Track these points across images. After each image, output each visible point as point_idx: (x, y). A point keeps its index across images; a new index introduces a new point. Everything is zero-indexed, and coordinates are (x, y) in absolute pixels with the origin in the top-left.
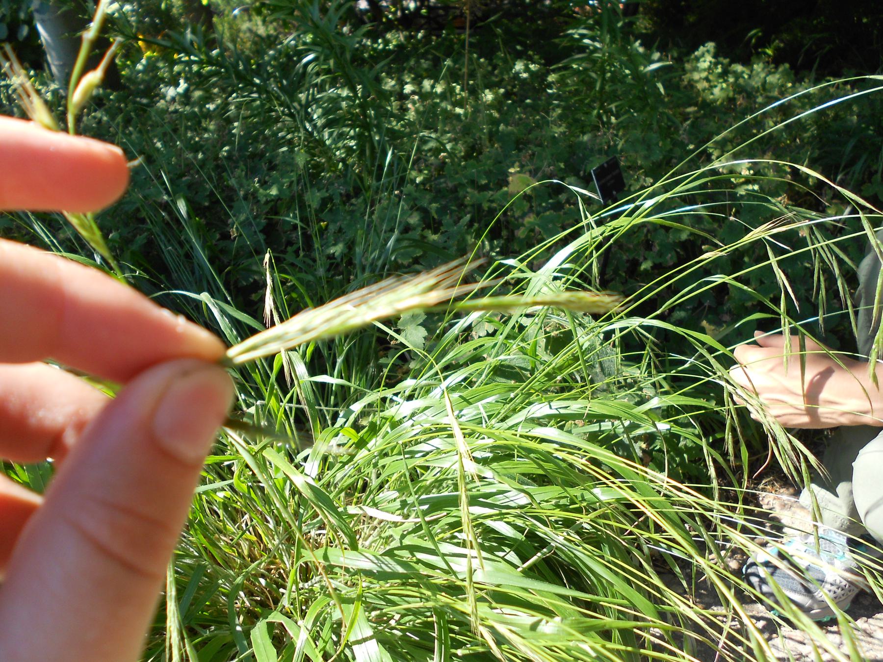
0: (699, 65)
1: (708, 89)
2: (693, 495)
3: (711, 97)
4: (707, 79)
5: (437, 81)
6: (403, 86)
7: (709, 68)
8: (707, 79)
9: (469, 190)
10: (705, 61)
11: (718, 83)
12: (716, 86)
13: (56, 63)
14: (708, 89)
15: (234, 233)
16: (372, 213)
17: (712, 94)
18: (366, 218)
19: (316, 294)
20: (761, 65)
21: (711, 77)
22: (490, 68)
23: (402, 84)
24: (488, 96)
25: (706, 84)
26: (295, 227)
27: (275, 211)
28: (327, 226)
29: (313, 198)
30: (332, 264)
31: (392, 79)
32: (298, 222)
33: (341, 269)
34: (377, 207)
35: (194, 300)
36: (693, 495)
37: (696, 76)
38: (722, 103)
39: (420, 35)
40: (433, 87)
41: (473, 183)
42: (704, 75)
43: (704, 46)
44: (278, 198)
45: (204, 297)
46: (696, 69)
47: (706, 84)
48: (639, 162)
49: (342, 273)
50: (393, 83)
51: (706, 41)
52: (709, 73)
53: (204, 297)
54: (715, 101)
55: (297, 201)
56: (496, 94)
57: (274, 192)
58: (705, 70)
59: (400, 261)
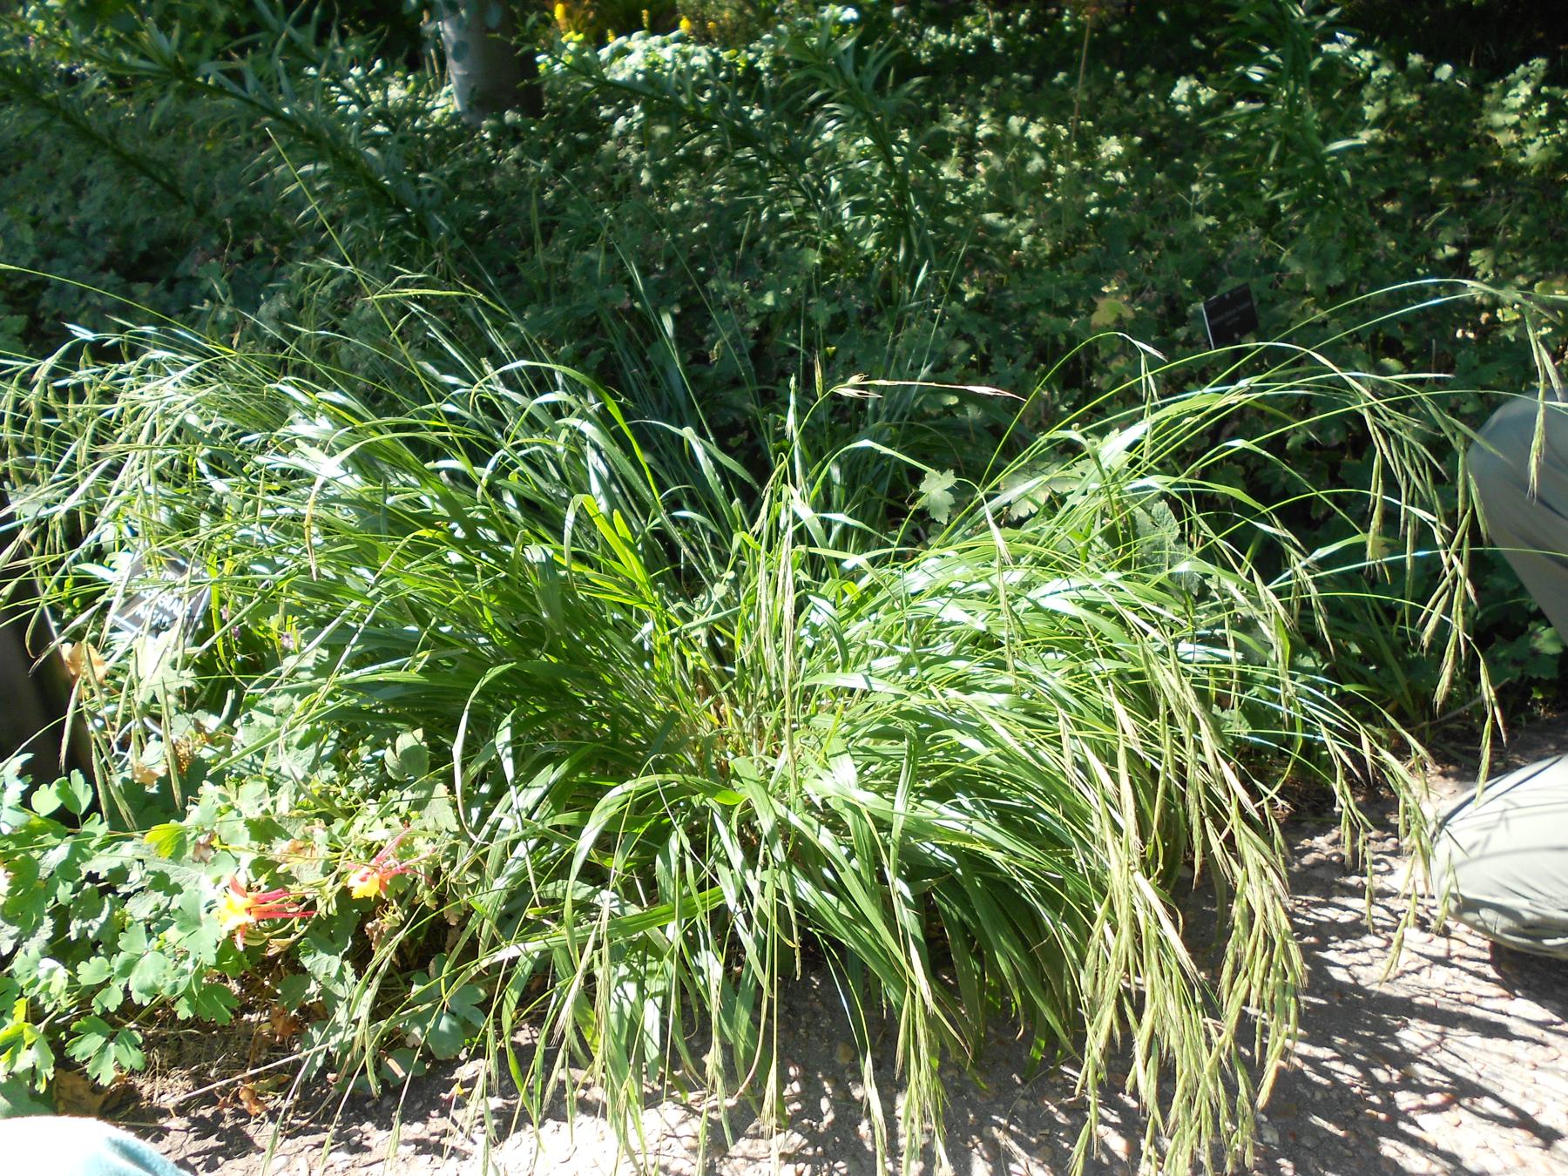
0: (1505, 101)
1: (1518, 147)
2: (1493, 1011)
3: (1521, 160)
4: (1517, 128)
5: (1032, 119)
6: (976, 125)
7: (1526, 107)
8: (1517, 128)
9: (1041, 314)
10: (1517, 95)
11: (1538, 134)
12: (1531, 142)
13: (459, 72)
14: (1518, 147)
15: (714, 355)
16: (895, 342)
17: (1523, 154)
18: (888, 347)
19: (814, 443)
20: (189, 684)
21: (1523, 124)
22: (1128, 93)
23: (976, 121)
24: (1112, 147)
25: (1512, 137)
26: (793, 352)
27: (766, 329)
28: (835, 352)
29: (822, 312)
30: (836, 407)
31: (958, 112)
32: (801, 349)
33: (848, 414)
34: (904, 332)
35: (673, 434)
36: (1493, 1011)
37: (1498, 118)
38: (1539, 173)
39: (1023, 17)
40: (1024, 128)
41: (1048, 304)
42: (1513, 118)
43: (1527, 65)
44: (773, 311)
45: (688, 433)
46: (1500, 107)
47: (1512, 137)
48: (1308, 286)
49: (849, 420)
50: (960, 119)
51: (1533, 56)
52: (1523, 117)
53: (688, 433)
54: (1524, 168)
55: (794, 314)
56: (1127, 144)
57: (769, 300)
58: (1515, 111)
59: (927, 410)
